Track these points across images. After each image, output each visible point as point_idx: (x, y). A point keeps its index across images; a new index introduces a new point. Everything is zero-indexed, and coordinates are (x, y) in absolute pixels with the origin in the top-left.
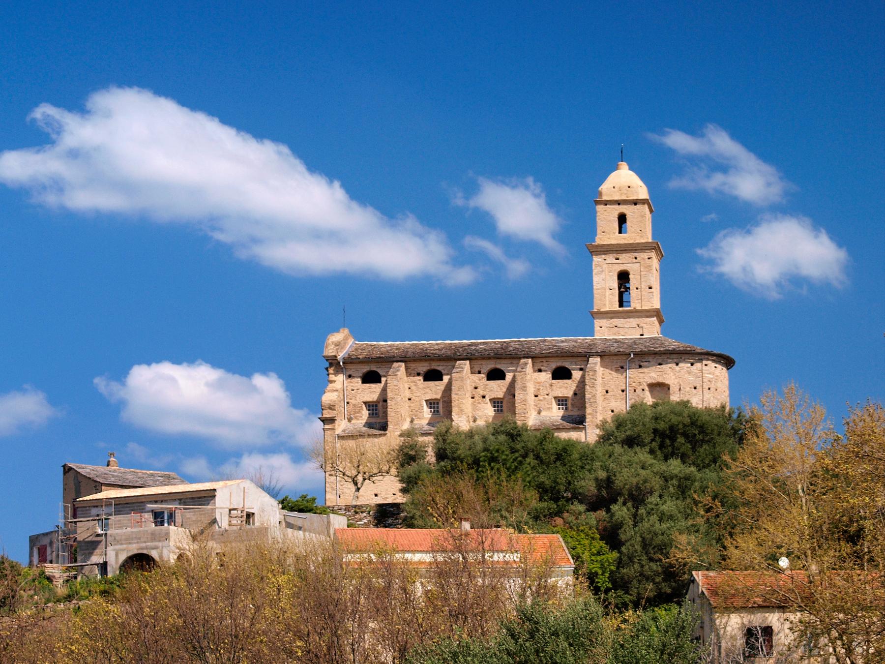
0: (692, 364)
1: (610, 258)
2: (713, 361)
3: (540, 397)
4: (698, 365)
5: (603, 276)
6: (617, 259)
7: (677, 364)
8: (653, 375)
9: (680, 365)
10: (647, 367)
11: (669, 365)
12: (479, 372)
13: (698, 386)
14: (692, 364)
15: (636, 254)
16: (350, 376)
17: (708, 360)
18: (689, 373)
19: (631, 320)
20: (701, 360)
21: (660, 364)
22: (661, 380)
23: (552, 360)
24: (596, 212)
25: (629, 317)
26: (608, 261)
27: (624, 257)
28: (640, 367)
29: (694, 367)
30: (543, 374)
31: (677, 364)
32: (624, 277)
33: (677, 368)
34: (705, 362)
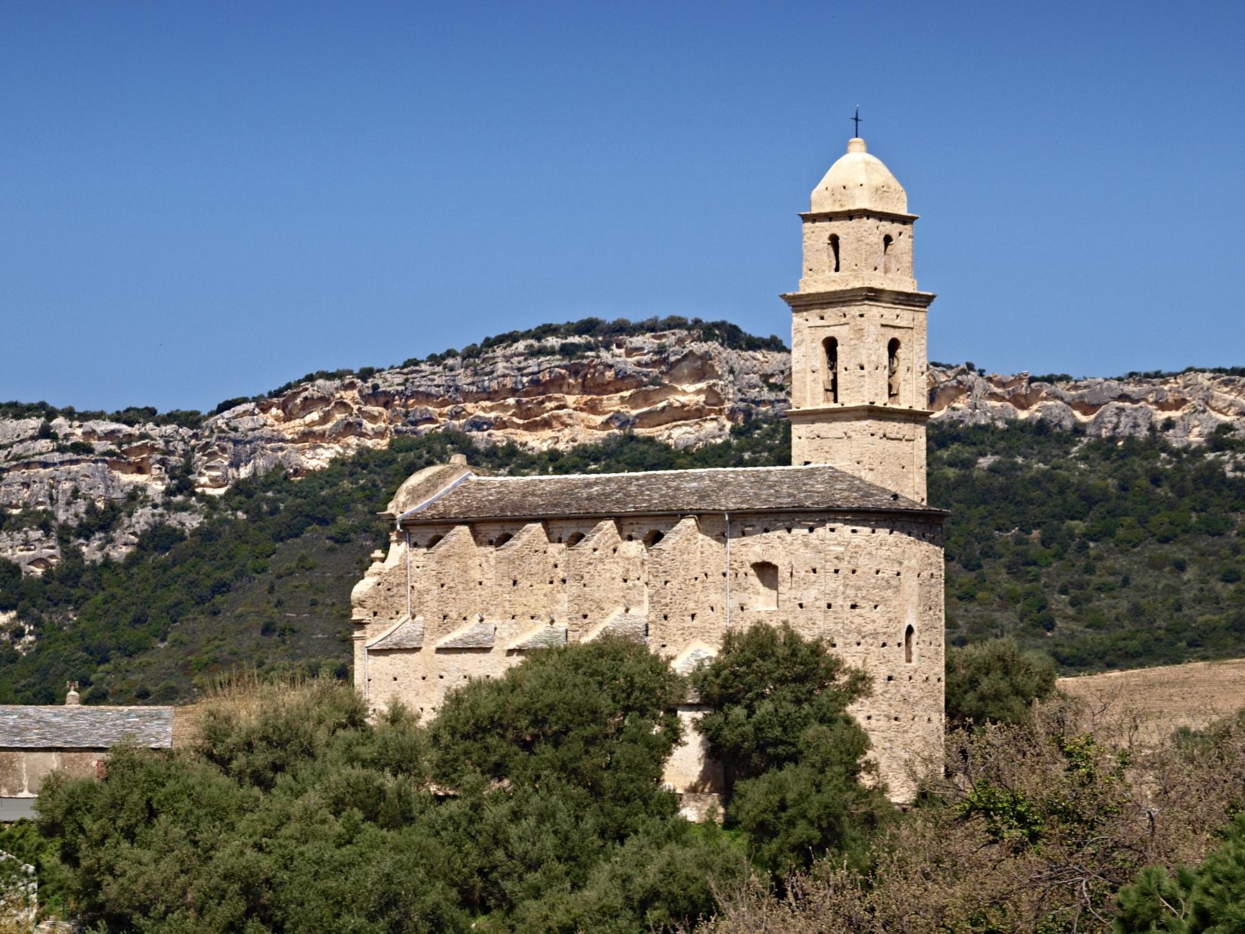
0: (811, 530)
1: (813, 317)
2: (846, 522)
3: (630, 583)
4: (820, 531)
5: (803, 349)
6: (822, 318)
7: (789, 531)
8: (757, 549)
9: (794, 531)
10: (751, 534)
11: (778, 533)
12: (560, 541)
13: (818, 567)
14: (811, 530)
15: (845, 309)
16: (415, 545)
17: (835, 521)
18: (806, 545)
19: (838, 424)
20: (822, 523)
21: (767, 531)
22: (767, 559)
23: (642, 521)
24: (802, 235)
25: (836, 420)
26: (810, 323)
27: (832, 314)
28: (744, 534)
29: (813, 535)
30: (634, 543)
31: (789, 531)
32: (831, 346)
33: (788, 537)
34: (829, 526)
